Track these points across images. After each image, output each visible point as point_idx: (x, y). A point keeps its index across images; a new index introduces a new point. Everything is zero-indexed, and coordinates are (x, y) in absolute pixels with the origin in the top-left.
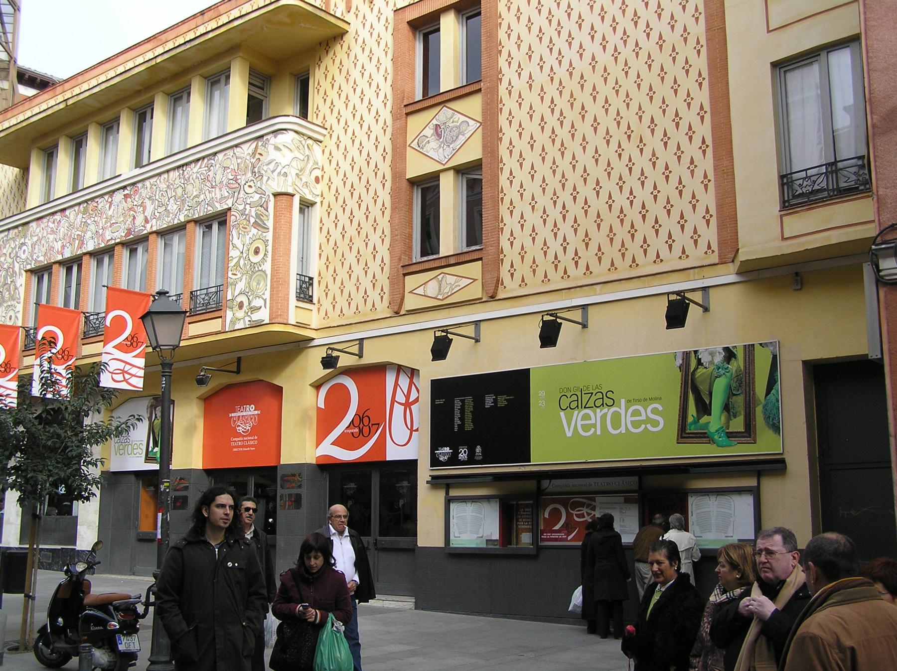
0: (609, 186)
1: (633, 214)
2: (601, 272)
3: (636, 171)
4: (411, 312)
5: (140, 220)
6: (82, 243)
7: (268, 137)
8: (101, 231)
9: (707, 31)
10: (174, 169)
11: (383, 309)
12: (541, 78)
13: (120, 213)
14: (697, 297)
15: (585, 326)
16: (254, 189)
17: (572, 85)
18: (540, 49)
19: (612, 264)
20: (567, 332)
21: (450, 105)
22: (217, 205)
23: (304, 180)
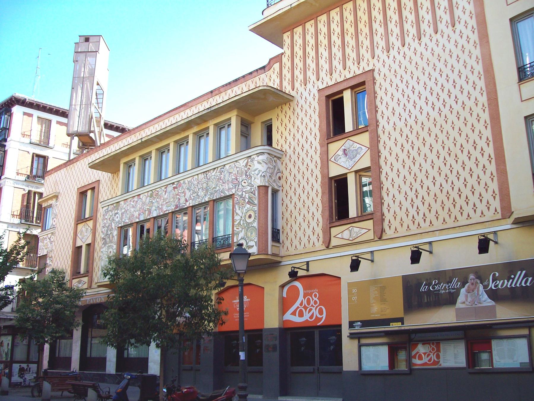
0: (440, 180)
1: (454, 194)
2: (438, 225)
3: (455, 172)
4: (335, 247)
5: (182, 200)
6: (150, 212)
7: (254, 156)
8: (160, 206)
9: (488, 100)
10: (201, 173)
11: (320, 245)
12: (400, 125)
13: (171, 197)
14: (491, 237)
15: (372, 261)
16: (247, 184)
17: (417, 128)
18: (399, 110)
19: (444, 220)
20: (363, 264)
21: (350, 138)
22: (227, 192)
23: (273, 179)
